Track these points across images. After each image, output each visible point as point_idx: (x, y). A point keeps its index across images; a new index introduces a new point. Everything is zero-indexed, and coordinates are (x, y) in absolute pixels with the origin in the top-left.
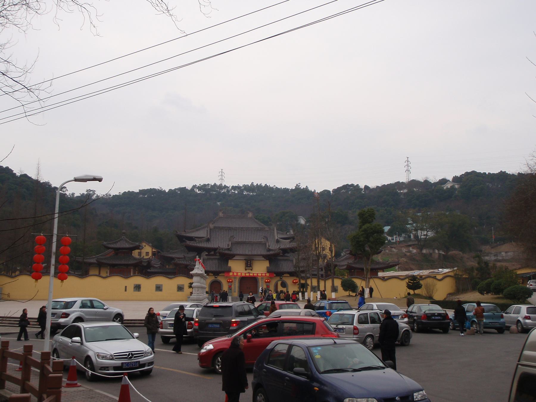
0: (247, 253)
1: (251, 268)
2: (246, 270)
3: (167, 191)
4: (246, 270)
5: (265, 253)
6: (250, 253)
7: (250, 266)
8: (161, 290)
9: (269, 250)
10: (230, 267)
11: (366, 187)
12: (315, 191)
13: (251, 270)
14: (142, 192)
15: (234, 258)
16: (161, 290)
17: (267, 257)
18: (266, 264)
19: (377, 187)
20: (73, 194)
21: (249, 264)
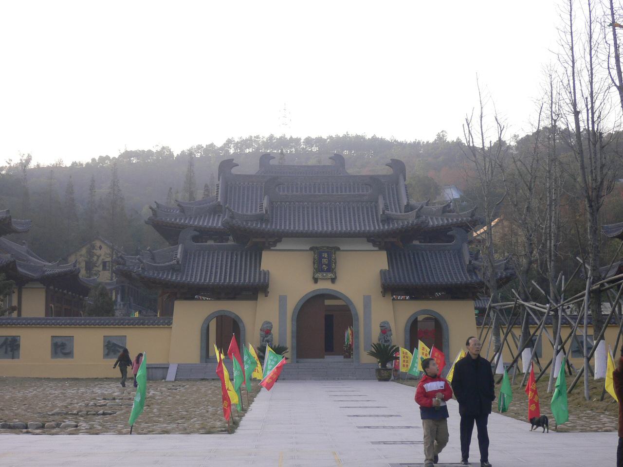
0: (319, 228)
1: (330, 275)
2: (316, 280)
3: (117, 157)
4: (316, 280)
5: (374, 226)
6: (327, 228)
7: (330, 269)
8: (69, 354)
9: (387, 219)
10: (266, 274)
11: (331, 137)
12: (93, 160)
13: (333, 280)
14: (374, 139)
15: (279, 246)
16: (69, 354)
17: (378, 240)
18: (379, 261)
19: (143, 151)
20: (178, 155)
21: (325, 264)
